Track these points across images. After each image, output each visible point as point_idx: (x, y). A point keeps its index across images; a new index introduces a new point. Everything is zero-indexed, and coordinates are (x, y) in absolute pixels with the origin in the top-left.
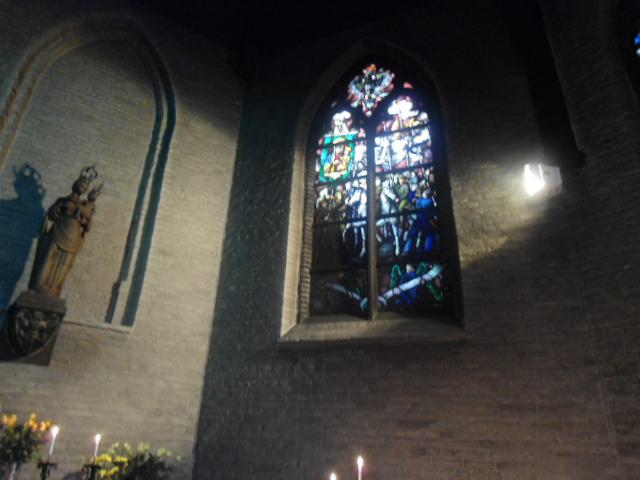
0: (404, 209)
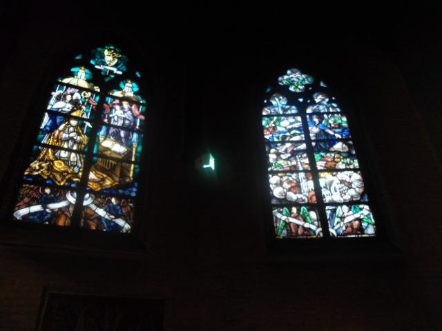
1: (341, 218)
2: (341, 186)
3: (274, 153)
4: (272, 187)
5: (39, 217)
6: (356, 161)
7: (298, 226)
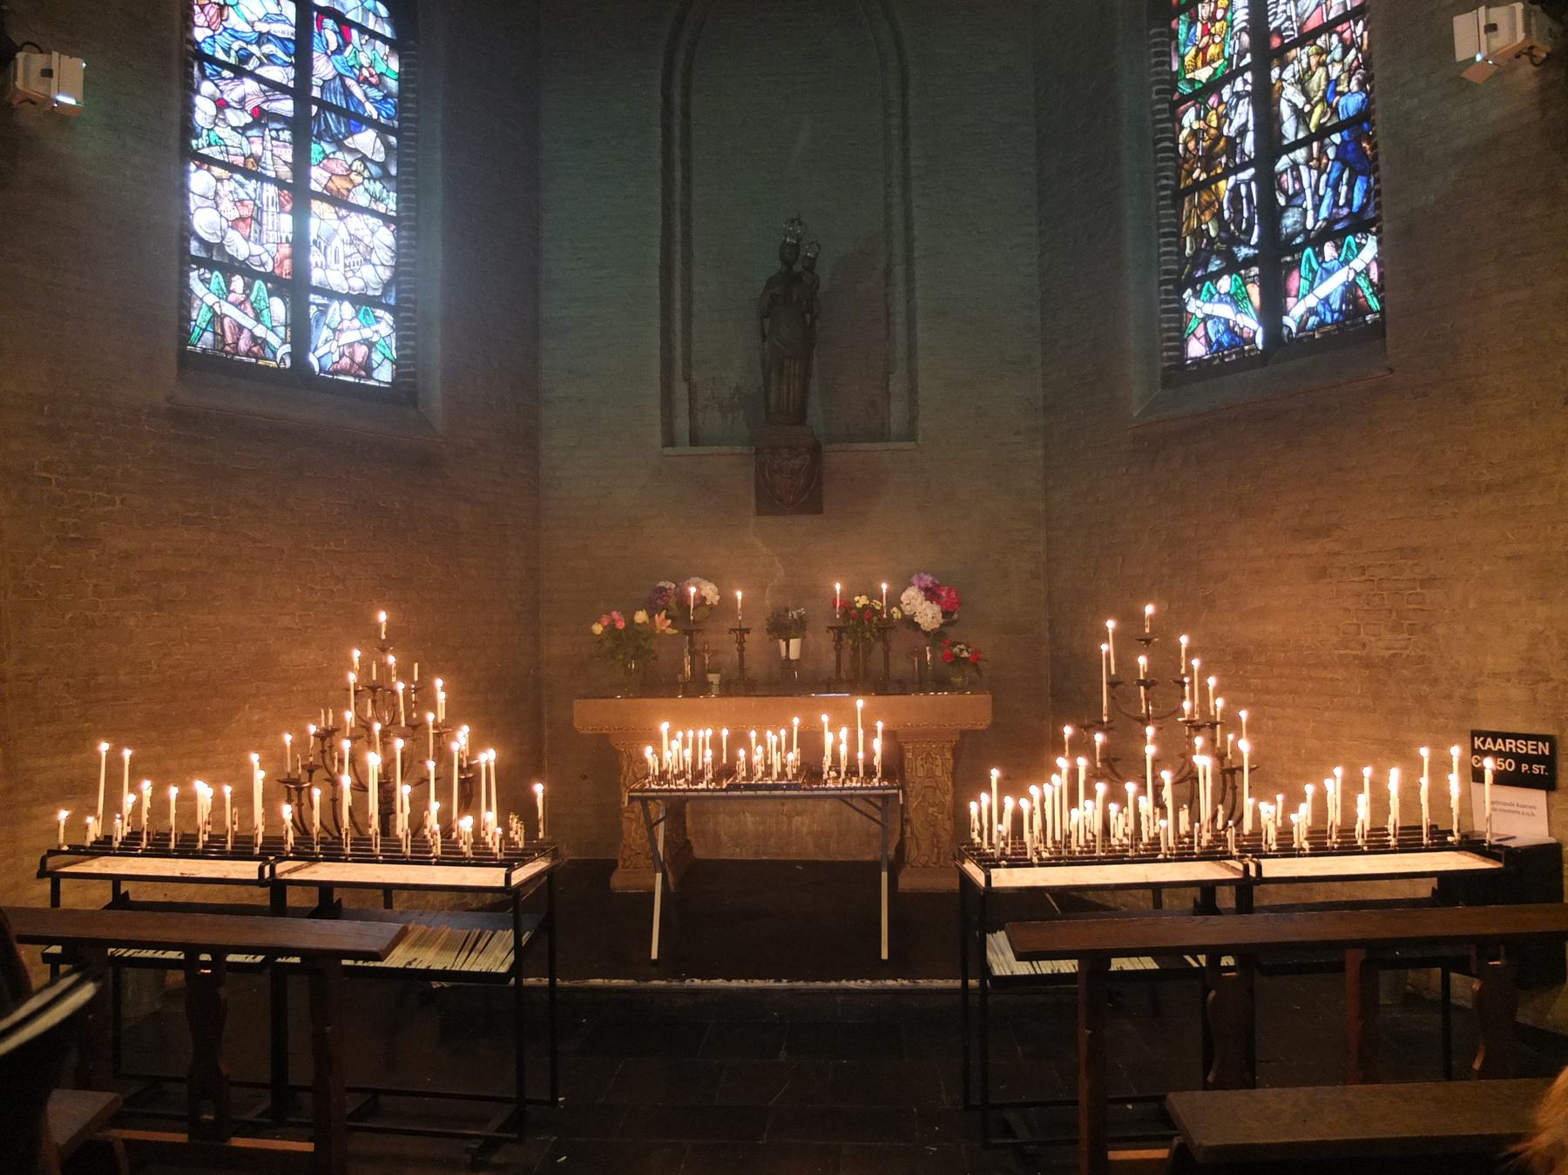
0: (1320, 126)
7: (241, 328)
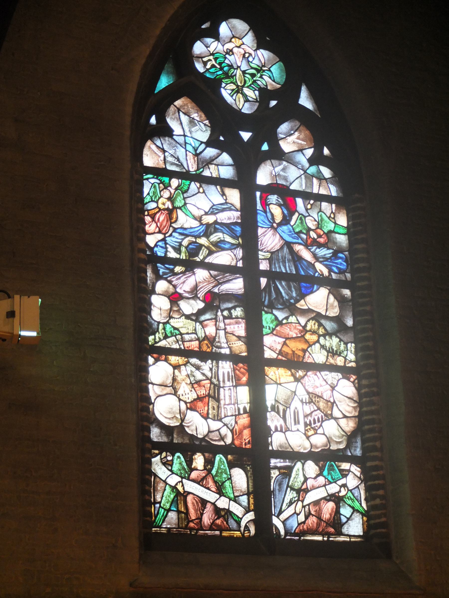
1: (298, 491)
2: (308, 409)
3: (165, 294)
4: (153, 391)
5: (154, 419)
6: (351, 346)
7: (204, 502)
